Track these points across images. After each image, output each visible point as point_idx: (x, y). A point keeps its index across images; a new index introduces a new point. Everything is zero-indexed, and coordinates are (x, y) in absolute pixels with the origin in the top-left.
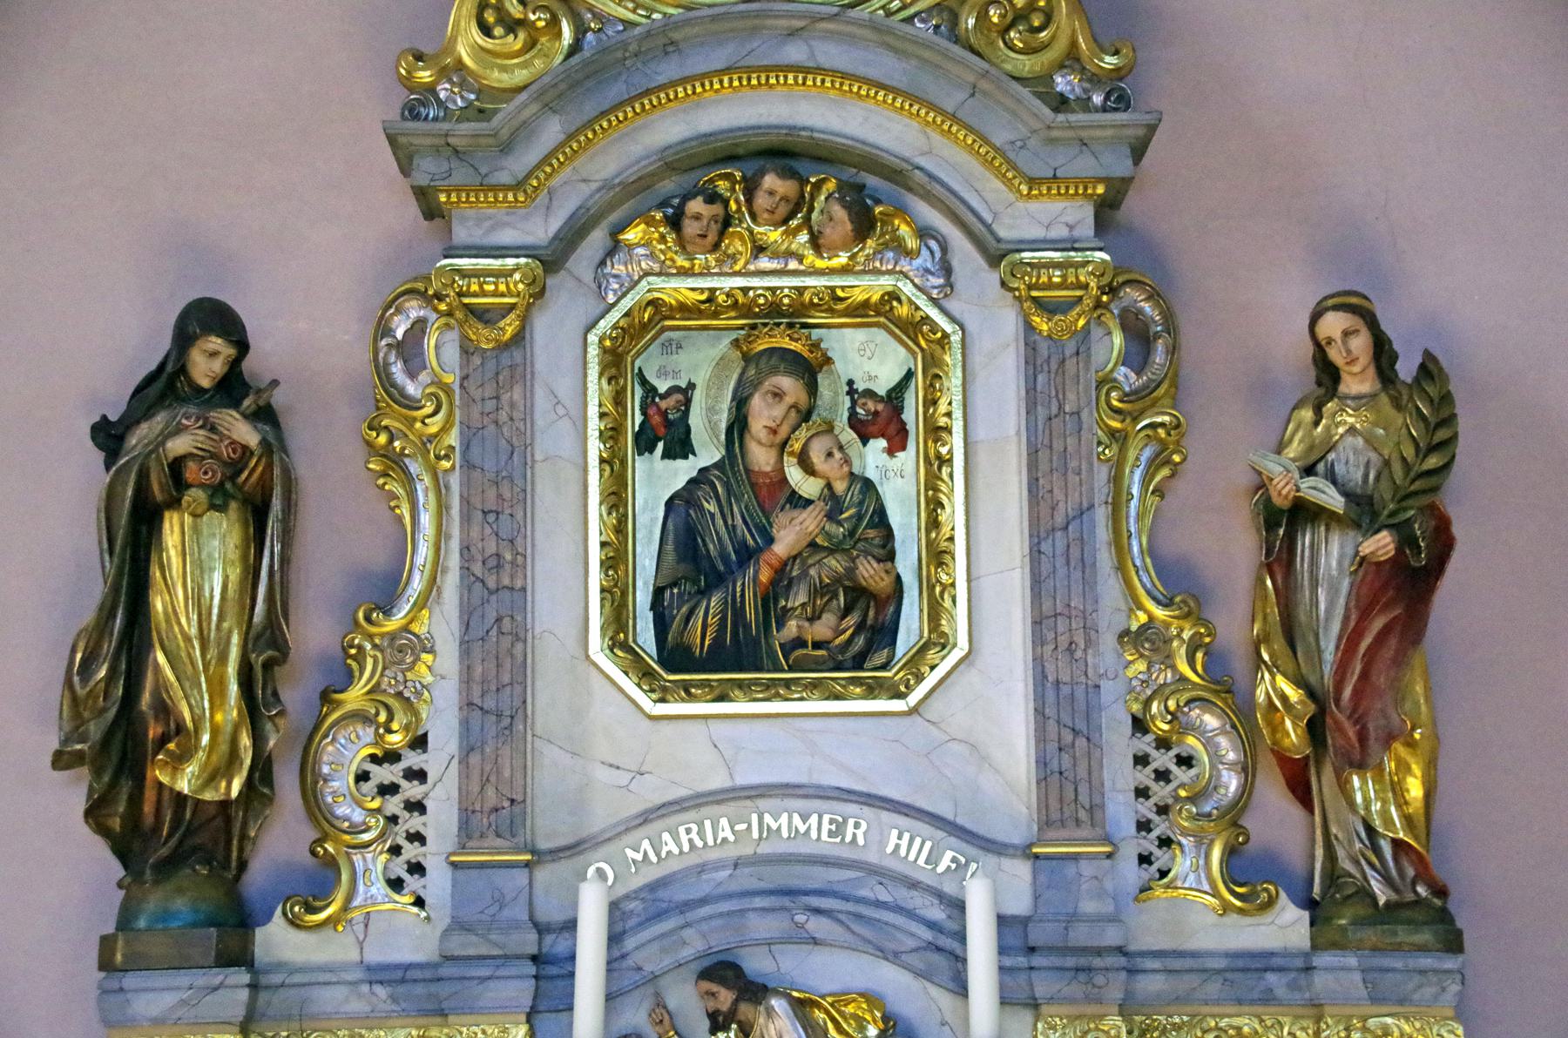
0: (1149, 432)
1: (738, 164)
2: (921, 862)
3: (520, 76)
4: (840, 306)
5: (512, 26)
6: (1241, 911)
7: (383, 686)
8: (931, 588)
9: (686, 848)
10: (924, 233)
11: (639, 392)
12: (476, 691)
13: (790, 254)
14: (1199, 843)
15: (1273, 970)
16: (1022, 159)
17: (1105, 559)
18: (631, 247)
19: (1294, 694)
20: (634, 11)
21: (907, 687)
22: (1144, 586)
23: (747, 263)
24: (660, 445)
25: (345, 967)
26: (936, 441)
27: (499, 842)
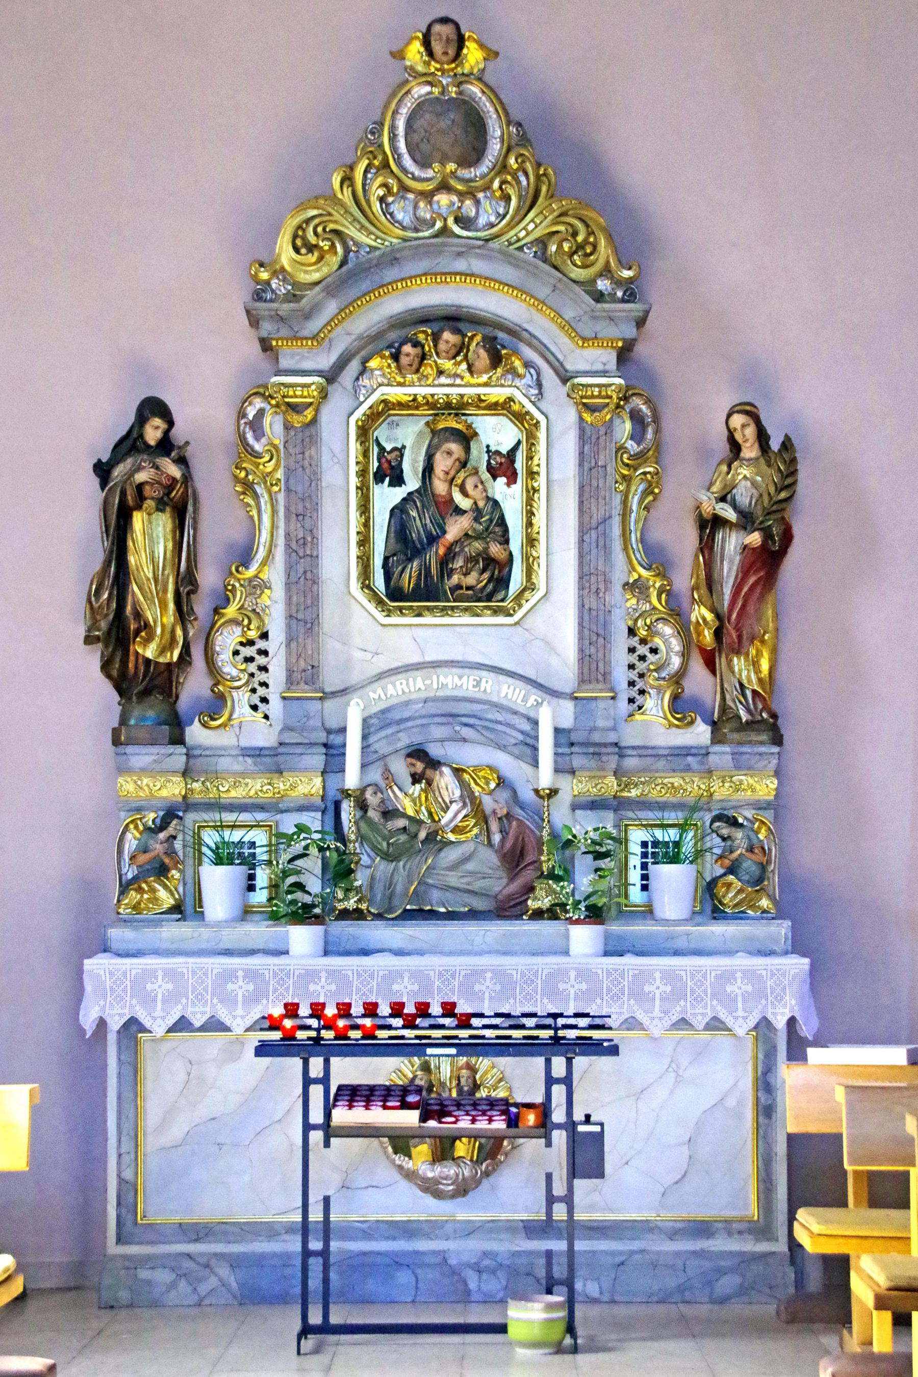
0: (643, 477)
1: (429, 324)
2: (519, 701)
3: (316, 276)
4: (483, 405)
5: (311, 248)
6: (677, 727)
7: (246, 606)
8: (528, 559)
9: (400, 693)
10: (527, 365)
11: (376, 450)
12: (294, 608)
13: (456, 375)
14: (659, 693)
15: (691, 755)
16: (580, 327)
17: (617, 545)
18: (372, 370)
19: (709, 616)
20: (375, 241)
21: (514, 611)
22: (637, 559)
23: (434, 380)
24: (387, 479)
25: (231, 748)
26: (532, 479)
27: (306, 687)
